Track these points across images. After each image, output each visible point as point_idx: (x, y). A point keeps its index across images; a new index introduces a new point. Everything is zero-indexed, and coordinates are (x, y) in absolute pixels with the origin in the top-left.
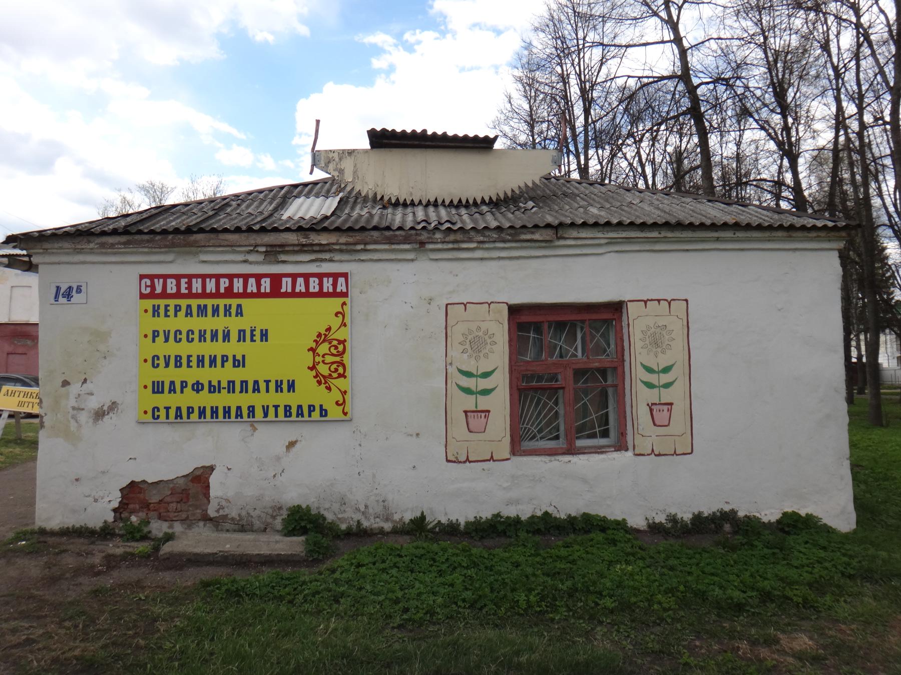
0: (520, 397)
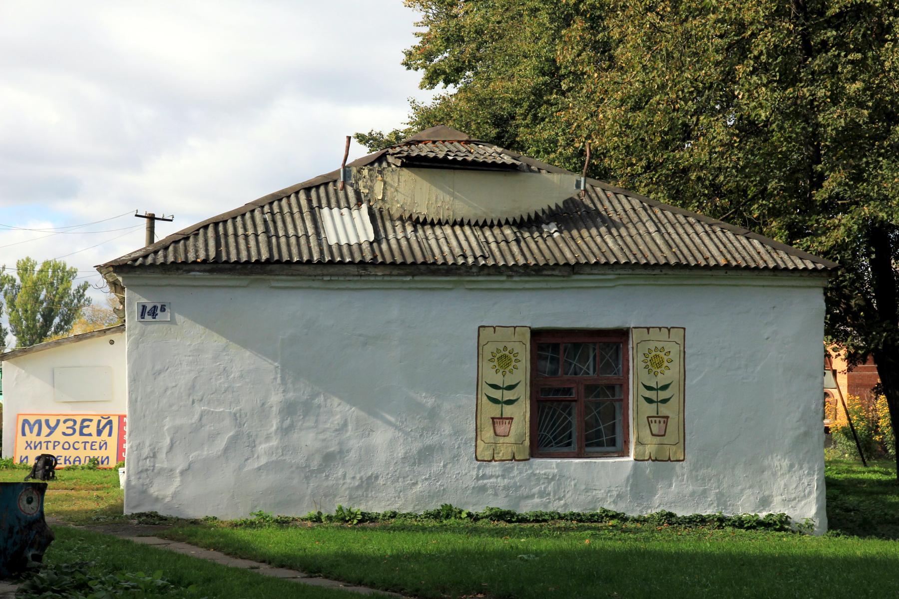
0: (539, 408)
